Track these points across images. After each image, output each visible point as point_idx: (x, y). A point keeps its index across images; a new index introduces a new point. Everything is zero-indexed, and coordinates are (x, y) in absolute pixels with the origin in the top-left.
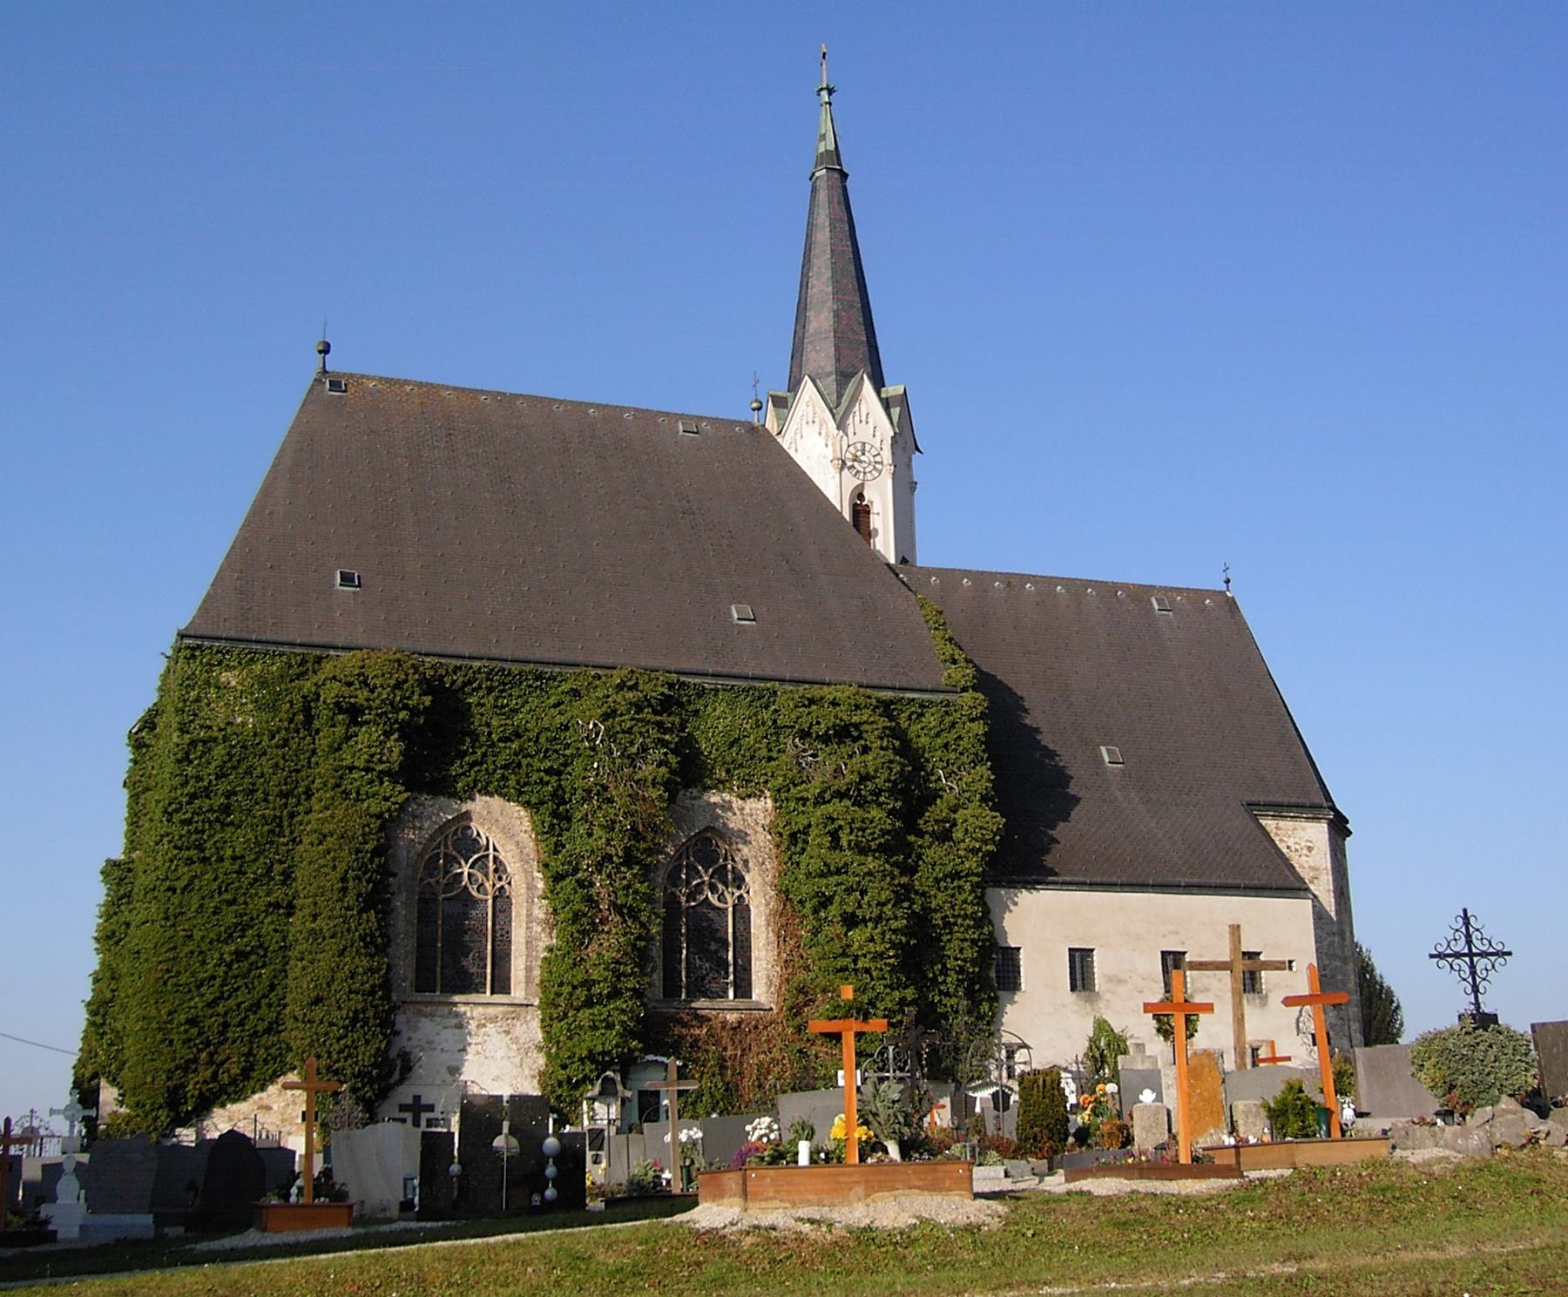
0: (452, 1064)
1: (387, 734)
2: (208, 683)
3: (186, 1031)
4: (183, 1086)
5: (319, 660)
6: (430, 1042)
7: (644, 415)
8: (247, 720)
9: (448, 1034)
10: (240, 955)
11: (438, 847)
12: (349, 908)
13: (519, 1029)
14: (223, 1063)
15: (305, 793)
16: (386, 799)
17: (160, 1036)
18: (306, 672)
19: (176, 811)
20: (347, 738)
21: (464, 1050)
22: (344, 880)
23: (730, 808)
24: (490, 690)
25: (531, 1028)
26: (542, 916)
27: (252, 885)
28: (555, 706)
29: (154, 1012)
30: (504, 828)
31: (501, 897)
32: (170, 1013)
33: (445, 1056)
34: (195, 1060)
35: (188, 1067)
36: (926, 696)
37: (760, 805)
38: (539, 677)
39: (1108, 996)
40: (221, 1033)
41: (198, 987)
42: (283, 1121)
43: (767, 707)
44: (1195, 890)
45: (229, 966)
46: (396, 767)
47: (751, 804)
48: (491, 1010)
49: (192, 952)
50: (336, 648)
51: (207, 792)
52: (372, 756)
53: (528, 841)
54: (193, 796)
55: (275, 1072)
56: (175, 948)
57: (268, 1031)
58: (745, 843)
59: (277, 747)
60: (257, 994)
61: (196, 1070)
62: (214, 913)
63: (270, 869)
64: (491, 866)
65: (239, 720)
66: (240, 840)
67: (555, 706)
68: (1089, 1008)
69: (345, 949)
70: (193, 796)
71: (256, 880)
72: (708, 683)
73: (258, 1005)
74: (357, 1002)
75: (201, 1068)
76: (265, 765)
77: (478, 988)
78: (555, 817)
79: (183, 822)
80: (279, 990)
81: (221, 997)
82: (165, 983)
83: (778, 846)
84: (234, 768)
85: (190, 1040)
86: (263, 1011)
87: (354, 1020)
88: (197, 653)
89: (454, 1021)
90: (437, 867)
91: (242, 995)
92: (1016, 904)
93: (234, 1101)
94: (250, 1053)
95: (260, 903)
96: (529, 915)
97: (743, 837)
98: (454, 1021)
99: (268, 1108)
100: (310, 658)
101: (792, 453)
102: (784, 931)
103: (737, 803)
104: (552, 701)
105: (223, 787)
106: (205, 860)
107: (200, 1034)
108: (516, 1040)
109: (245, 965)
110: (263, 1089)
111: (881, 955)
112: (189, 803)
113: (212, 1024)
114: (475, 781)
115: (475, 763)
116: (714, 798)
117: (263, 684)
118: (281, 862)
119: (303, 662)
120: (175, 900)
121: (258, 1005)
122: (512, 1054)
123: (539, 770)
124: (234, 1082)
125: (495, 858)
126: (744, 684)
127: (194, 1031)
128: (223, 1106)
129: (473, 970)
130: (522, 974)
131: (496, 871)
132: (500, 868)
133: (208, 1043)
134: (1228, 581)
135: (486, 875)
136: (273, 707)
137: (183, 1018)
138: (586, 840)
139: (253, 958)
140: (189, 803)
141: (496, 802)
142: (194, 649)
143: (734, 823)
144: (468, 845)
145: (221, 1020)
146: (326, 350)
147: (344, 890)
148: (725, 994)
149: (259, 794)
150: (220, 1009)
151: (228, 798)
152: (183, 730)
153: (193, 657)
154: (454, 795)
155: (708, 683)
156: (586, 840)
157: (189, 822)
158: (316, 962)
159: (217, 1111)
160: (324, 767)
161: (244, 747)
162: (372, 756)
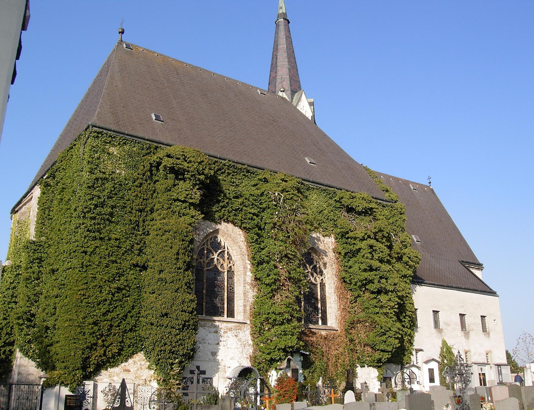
0: (213, 351)
1: (194, 185)
2: (103, 151)
3: (92, 328)
4: (89, 358)
5: (156, 148)
6: (203, 340)
7: (244, 84)
8: (122, 172)
9: (211, 336)
10: (119, 289)
11: (204, 245)
12: (179, 269)
13: (241, 335)
14: (108, 347)
15: (150, 210)
16: (192, 217)
17: (79, 330)
18: (150, 153)
19: (88, 212)
20: (175, 185)
21: (218, 344)
22: (178, 254)
23: (319, 240)
24: (229, 174)
25: (246, 334)
26: (250, 281)
27: (123, 254)
28: (255, 185)
29: (75, 317)
30: (232, 239)
31: (231, 272)
32: (84, 318)
33: (210, 346)
34: (96, 344)
35: (92, 347)
36: (385, 203)
37: (330, 240)
38: (248, 171)
39: (445, 331)
40: (109, 330)
41: (98, 305)
42: (136, 378)
43: (331, 198)
44: (466, 290)
45: (113, 295)
46: (198, 202)
47: (327, 239)
48: (230, 325)
49: (96, 286)
50: (163, 144)
51: (103, 205)
52: (187, 195)
53: (243, 245)
54: (96, 206)
55: (133, 351)
56: (87, 283)
57: (131, 330)
58: (326, 256)
59: (137, 186)
60: (127, 309)
61: (96, 349)
62: (106, 267)
63: (132, 246)
64: (226, 256)
65: (118, 171)
66: (118, 230)
67: (255, 185)
68: (440, 336)
69: (178, 289)
70: (96, 206)
71: (126, 252)
72: (311, 185)
73: (126, 316)
74: (186, 316)
75: (98, 348)
76: (130, 195)
77: (221, 314)
78: (256, 235)
79: (92, 218)
80: (136, 309)
81: (109, 311)
82: (81, 302)
83: (337, 259)
84: (116, 194)
85: (94, 333)
86: (129, 319)
87: (184, 326)
88: (100, 135)
89: (214, 330)
90: (203, 254)
91: (118, 311)
92: (416, 291)
93: (112, 367)
94: (122, 342)
95: (126, 264)
96: (244, 280)
97: (325, 253)
98: (214, 330)
99: (129, 371)
100: (154, 146)
101: (301, 111)
102: (341, 297)
103: (322, 238)
104: (253, 183)
105: (111, 203)
106: (101, 239)
107: (99, 330)
108: (240, 340)
109: (120, 295)
110: (126, 361)
111: (392, 308)
112: (94, 209)
113: (105, 325)
114: (224, 215)
115: (223, 207)
116: (314, 235)
117: (130, 156)
118: (138, 244)
119: (150, 148)
120: (87, 257)
121: (126, 316)
122: (239, 346)
123: (250, 213)
124: (113, 356)
125: (228, 253)
126: (324, 188)
127: (96, 328)
128: (107, 369)
129: (219, 305)
130: (241, 309)
131: (228, 258)
132: (230, 258)
133: (102, 335)
134: (430, 183)
135: (224, 260)
136: (135, 167)
137: (91, 321)
138: (274, 246)
139: (124, 291)
140: (94, 209)
141: (230, 226)
142: (98, 133)
143: (321, 247)
144: (217, 246)
145: (109, 323)
146: (122, 32)
147: (177, 259)
148: (317, 323)
149: (128, 209)
150: (109, 317)
151: (112, 209)
152: (91, 172)
153: (97, 137)
154: (214, 221)
155: (311, 185)
156: (274, 246)
157: (94, 218)
158: (162, 294)
159: (103, 372)
160: (163, 198)
161: (121, 185)
162: (187, 195)
